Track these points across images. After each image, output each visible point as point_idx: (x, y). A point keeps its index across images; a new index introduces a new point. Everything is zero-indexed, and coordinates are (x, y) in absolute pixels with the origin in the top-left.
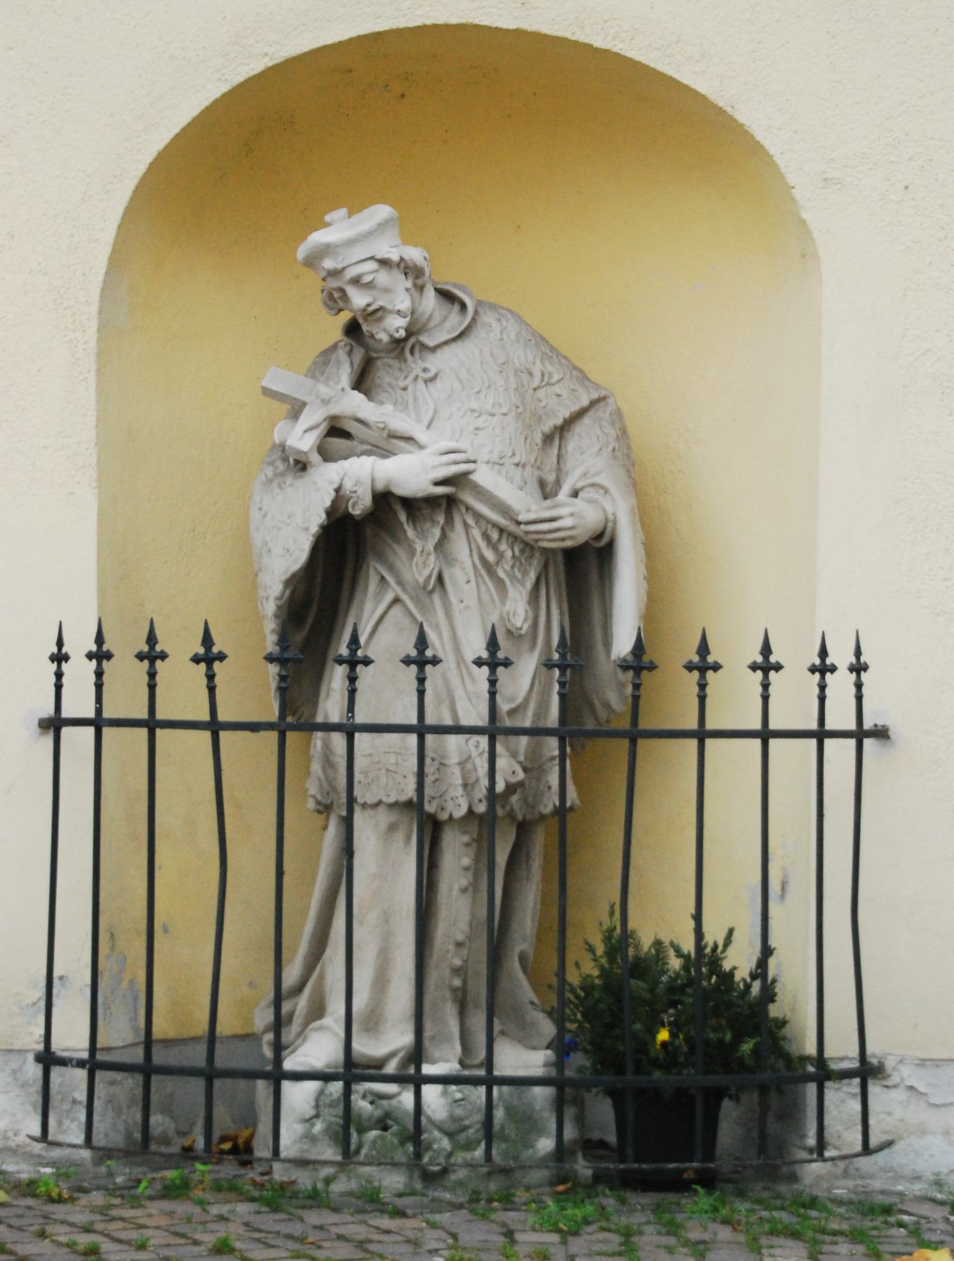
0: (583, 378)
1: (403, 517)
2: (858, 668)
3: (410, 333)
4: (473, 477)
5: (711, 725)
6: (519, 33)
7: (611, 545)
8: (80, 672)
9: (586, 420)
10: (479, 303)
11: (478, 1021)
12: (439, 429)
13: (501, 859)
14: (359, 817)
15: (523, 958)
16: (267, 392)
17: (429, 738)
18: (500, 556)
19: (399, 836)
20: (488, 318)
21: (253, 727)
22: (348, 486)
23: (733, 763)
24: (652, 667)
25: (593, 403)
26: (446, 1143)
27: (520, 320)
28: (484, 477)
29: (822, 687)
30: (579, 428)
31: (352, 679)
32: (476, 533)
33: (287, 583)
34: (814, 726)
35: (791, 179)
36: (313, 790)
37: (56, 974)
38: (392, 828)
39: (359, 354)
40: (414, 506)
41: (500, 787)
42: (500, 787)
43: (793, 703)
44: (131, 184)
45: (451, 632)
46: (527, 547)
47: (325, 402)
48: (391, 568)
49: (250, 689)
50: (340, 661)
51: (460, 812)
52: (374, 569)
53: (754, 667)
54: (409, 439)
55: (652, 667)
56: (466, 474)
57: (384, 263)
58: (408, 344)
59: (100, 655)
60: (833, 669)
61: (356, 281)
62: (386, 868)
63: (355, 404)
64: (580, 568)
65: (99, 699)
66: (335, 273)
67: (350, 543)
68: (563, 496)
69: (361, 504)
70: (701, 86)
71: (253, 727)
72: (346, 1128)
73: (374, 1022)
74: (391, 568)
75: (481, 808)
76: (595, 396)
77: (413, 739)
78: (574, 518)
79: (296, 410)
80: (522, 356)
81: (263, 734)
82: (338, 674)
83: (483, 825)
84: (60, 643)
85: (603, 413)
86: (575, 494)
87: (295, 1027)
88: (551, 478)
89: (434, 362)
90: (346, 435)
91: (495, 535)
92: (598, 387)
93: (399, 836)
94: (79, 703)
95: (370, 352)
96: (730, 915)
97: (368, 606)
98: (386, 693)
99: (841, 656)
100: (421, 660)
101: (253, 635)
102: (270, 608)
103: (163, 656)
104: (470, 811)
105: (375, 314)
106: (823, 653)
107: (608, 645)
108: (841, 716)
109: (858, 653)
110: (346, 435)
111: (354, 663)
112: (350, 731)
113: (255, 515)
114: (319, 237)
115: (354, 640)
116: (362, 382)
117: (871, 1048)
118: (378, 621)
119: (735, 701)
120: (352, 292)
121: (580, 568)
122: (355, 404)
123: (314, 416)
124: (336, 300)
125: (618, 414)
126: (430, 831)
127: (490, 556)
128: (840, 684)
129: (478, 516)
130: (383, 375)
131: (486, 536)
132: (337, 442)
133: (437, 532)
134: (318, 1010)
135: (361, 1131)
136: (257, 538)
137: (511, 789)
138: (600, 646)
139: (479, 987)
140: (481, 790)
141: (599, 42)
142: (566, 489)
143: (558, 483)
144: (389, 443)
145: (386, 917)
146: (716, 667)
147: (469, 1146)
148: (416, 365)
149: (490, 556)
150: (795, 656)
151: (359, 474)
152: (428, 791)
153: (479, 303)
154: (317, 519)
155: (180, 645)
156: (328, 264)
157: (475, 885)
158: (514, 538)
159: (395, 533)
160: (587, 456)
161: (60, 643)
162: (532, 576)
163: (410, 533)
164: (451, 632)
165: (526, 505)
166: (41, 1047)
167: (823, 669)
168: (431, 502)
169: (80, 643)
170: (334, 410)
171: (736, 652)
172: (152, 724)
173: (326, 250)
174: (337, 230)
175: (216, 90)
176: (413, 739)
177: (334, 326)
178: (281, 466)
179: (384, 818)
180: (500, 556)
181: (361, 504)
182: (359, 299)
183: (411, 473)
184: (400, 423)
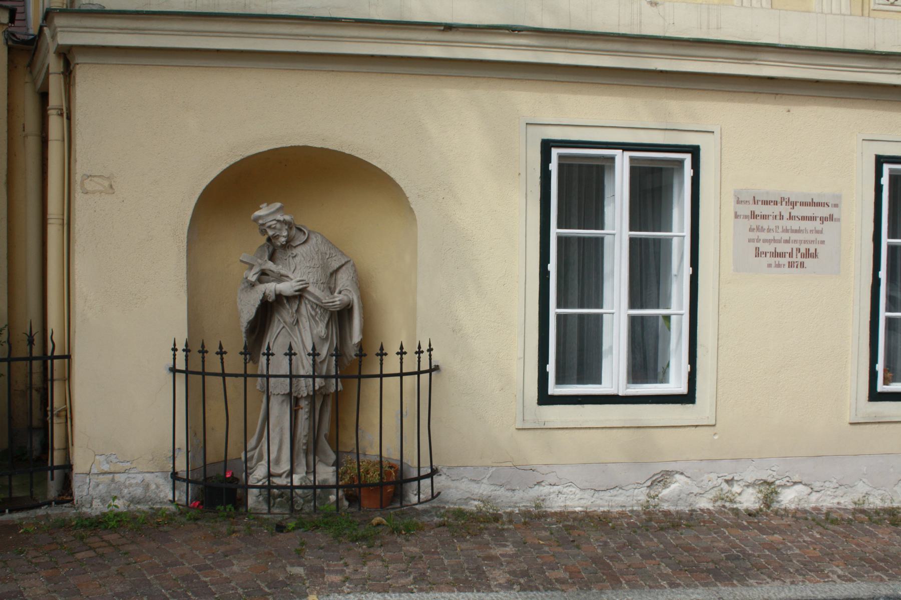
0: (343, 254)
1: (285, 301)
2: (430, 350)
3: (287, 242)
4: (309, 289)
5: (384, 372)
6: (322, 148)
7: (352, 307)
8: (181, 355)
9: (344, 268)
10: (309, 232)
11: (311, 458)
12: (296, 273)
13: (318, 407)
14: (272, 399)
15: (325, 436)
16: (241, 261)
17: (294, 379)
18: (316, 313)
19: (285, 404)
20: (312, 236)
21: (236, 376)
22: (267, 292)
23: (392, 384)
24: (365, 355)
25: (346, 263)
26: (302, 501)
27: (322, 236)
28: (311, 289)
29: (419, 358)
30: (341, 271)
31: (268, 360)
32: (309, 306)
33: (249, 323)
34: (416, 370)
35: (408, 195)
36: (258, 388)
37: (176, 447)
38: (283, 401)
39: (271, 249)
40: (289, 299)
41: (317, 388)
42: (317, 388)
43: (410, 364)
44: (197, 196)
45: (300, 339)
46: (325, 309)
47: (260, 265)
48: (282, 317)
49: (234, 362)
50: (264, 354)
51: (305, 395)
52: (277, 317)
53: (398, 353)
54: (287, 277)
55: (365, 355)
56: (306, 288)
57: (278, 221)
58: (288, 245)
59: (187, 350)
60: (422, 352)
61: (269, 227)
62: (280, 413)
63: (270, 265)
64: (341, 317)
65: (187, 365)
66: (263, 225)
67: (268, 310)
68: (336, 294)
69: (272, 298)
70: (379, 166)
71: (236, 376)
72: (269, 499)
73: (278, 461)
74: (282, 317)
75: (311, 393)
76: (346, 260)
77: (288, 380)
78: (338, 299)
79: (251, 266)
80: (323, 248)
81: (239, 378)
82: (263, 359)
83: (312, 398)
84: (175, 345)
85: (349, 265)
86: (340, 293)
87: (254, 461)
88: (333, 286)
89: (295, 252)
90: (267, 275)
91: (315, 306)
92: (347, 257)
93: (285, 404)
94: (181, 365)
95: (275, 249)
96: (391, 452)
97: (275, 329)
98: (280, 365)
99: (425, 347)
100: (290, 353)
101: (236, 342)
102: (244, 330)
103: (207, 352)
104: (308, 395)
105: (276, 237)
106: (419, 347)
107: (351, 337)
108: (425, 366)
109: (430, 345)
110: (267, 275)
111: (269, 354)
112: (268, 377)
113: (238, 300)
114: (258, 213)
115: (269, 348)
116: (272, 258)
117: (434, 464)
118: (277, 338)
119: (392, 364)
120: (268, 230)
121: (341, 317)
122: (270, 265)
123: (256, 269)
124: (264, 232)
125: (354, 265)
126: (294, 401)
127: (313, 313)
128: (425, 356)
129: (309, 301)
130: (278, 255)
131: (312, 307)
132: (264, 277)
133: (296, 307)
134: (260, 458)
135: (275, 499)
136: (240, 307)
137: (320, 388)
138: (349, 339)
139: (311, 446)
140: (311, 388)
141: (347, 152)
142: (337, 291)
143: (335, 288)
144: (281, 278)
145: (282, 429)
146: (386, 354)
147: (309, 501)
148: (289, 253)
149: (313, 313)
150: (410, 349)
151: (271, 288)
152: (293, 390)
153: (309, 232)
154: (258, 303)
155: (213, 348)
156: (261, 222)
157: (310, 416)
158: (321, 307)
159: (282, 305)
160: (344, 279)
161: (175, 345)
162: (327, 319)
163: (288, 306)
164: (300, 339)
165: (325, 298)
166: (172, 470)
167: (419, 352)
168: (294, 297)
169: (181, 346)
170: (263, 267)
171: (392, 349)
172: (204, 374)
173: (260, 217)
174: (263, 211)
175: (224, 166)
176: (288, 380)
177: (263, 240)
178: (246, 284)
179: (280, 399)
180: (316, 313)
181: (272, 298)
182: (271, 233)
183: (287, 287)
184: (283, 272)
